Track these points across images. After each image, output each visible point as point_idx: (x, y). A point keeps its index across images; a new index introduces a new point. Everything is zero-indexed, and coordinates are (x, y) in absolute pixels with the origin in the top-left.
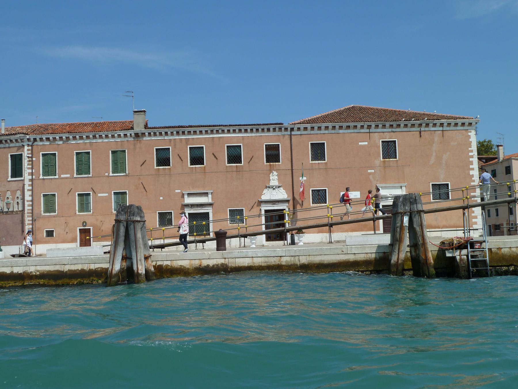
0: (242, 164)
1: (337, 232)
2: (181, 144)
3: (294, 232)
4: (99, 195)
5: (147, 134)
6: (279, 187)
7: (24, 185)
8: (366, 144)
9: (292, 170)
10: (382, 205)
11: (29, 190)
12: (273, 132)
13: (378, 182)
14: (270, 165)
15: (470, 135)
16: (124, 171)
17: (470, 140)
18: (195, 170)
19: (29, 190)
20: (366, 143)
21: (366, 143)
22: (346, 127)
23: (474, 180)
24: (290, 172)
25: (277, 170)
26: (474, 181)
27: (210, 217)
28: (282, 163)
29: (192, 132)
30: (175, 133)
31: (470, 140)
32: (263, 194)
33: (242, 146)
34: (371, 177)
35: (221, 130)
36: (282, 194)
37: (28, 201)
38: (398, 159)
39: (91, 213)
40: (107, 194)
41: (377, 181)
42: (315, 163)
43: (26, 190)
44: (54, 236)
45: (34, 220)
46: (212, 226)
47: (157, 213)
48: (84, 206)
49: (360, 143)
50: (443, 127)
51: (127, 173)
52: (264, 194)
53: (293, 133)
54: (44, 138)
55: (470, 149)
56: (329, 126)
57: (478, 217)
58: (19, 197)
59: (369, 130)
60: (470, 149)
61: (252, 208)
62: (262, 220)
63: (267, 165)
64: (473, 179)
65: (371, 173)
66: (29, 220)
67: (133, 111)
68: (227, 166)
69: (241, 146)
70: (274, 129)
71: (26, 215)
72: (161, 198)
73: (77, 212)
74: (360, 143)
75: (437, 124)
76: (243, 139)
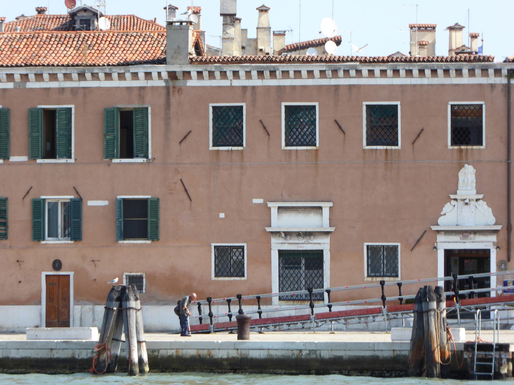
0: (399, 147)
6: (477, 200)
14: (461, 151)
18: (297, 156)
28: (486, 146)
32: (442, 213)
51: (150, 157)
52: (445, 214)
61: (416, 245)
68: (364, 150)
72: (222, 215)
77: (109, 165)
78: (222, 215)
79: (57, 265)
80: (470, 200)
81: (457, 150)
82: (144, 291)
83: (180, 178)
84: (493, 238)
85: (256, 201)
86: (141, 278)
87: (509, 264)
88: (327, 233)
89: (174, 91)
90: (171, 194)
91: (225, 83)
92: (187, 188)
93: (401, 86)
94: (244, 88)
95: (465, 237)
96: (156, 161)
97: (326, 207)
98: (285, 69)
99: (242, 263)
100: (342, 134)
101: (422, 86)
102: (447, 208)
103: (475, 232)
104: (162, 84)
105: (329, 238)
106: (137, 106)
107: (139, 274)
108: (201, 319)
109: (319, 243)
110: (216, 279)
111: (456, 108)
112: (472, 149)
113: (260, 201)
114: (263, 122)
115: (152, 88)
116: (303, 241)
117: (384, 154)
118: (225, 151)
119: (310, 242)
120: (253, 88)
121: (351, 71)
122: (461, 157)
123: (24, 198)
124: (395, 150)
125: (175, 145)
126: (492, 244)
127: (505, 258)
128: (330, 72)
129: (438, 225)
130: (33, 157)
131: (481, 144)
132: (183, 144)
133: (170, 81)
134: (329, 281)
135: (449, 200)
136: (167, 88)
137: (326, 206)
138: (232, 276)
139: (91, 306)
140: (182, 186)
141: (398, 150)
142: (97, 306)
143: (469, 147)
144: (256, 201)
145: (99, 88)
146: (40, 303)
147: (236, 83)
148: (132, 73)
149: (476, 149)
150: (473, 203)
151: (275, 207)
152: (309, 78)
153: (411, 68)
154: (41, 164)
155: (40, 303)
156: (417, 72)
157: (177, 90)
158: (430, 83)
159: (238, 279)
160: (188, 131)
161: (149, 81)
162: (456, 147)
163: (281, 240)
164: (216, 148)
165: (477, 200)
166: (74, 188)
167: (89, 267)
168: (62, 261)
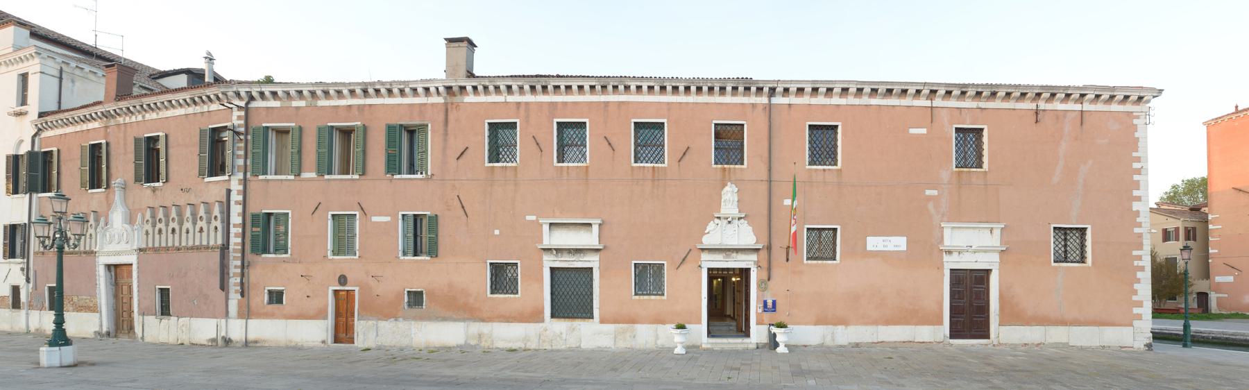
0: (665, 165)
1: (856, 325)
2: (539, 114)
3: (764, 254)
4: (375, 219)
5: (469, 88)
6: (739, 219)
7: (229, 191)
8: (923, 132)
9: (770, 181)
10: (951, 270)
11: (237, 203)
12: (13, 310)
13: (945, 219)
14: (724, 169)
15: (1136, 125)
16: (423, 169)
17: (1137, 135)
18: (568, 172)
19: (237, 203)
20: (924, 131)
21: (924, 131)
22: (885, 90)
23: (1141, 223)
24: (763, 187)
25: (737, 182)
26: (1140, 225)
27: (594, 278)
28: (748, 165)
29: (563, 88)
30: (527, 87)
31: (1137, 135)
32: (706, 232)
33: (666, 125)
34: (931, 206)
35: (623, 87)
36: (744, 235)
37: (235, 226)
38: (987, 170)
39: (357, 257)
40: (387, 219)
41: (943, 215)
42: (816, 170)
43: (232, 203)
44: (284, 302)
45: (246, 265)
46: (598, 298)
47: (488, 264)
48: (343, 244)
49: (912, 131)
50: (1082, 103)
51: (429, 173)
52: (708, 233)
53: (775, 100)
54: (267, 94)
55: (1135, 154)
56: (851, 86)
57: (1145, 303)
58: (174, 227)
59: (932, 103)
60: (1135, 154)
61: (681, 263)
62: (702, 291)
63: (716, 168)
64: (1138, 220)
65: (930, 198)
66: (236, 267)
67: (446, 39)
68: (632, 167)
69: (663, 123)
70: (772, 91)
71: (232, 255)
72: (497, 232)
73: (329, 253)
74: (912, 131)
75: (819, 89)
76: (669, 110)
77: (391, 180)
78: (497, 232)
79: (343, 280)
80: (732, 219)
81: (721, 168)
82: (424, 307)
83: (457, 194)
84: (754, 257)
85: (529, 218)
86: (421, 293)
87: (769, 283)
88: (597, 250)
89: (452, 108)
90: (449, 210)
91: (500, 99)
92: (464, 205)
93: (668, 103)
94: (518, 104)
95: (728, 256)
96: (435, 178)
97: (595, 224)
98: (556, 84)
99: (516, 280)
100: (612, 151)
101: (687, 103)
102: (711, 226)
103: (737, 250)
104: (440, 100)
105: (598, 256)
106: (417, 122)
107: (419, 290)
108: (1065, 240)
109: (589, 261)
110: (492, 296)
111: (719, 128)
112: (735, 168)
113: (533, 218)
114: (536, 137)
115: (433, 105)
116: (573, 259)
117: (651, 171)
118: (500, 167)
119: (581, 259)
120: (527, 104)
121: (619, 87)
122: (724, 176)
123: (313, 213)
124: (662, 167)
125: (452, 161)
126: (753, 263)
127: (766, 278)
128: (600, 87)
129: (702, 243)
130: (320, 173)
131: (742, 163)
132: (460, 160)
133: (448, 97)
134: (916, 132)
135: (713, 218)
136: (446, 104)
137: (596, 222)
138: (507, 293)
139: (375, 322)
140: (459, 202)
141: (665, 167)
142: (380, 322)
143: (732, 166)
144: (529, 218)
145: (383, 105)
146: (325, 318)
147: (511, 99)
148: (411, 88)
149: (738, 168)
150: (736, 222)
151: (546, 223)
152: (579, 94)
153: (678, 84)
154: (329, 180)
155: (940, 323)
156: (683, 88)
157: (454, 106)
158: (695, 101)
159: (512, 296)
160: (465, 148)
161: (429, 98)
162: (719, 166)
163: (553, 258)
164: (491, 165)
165: (739, 219)
166: (359, 203)
167: (373, 283)
168: (347, 276)
